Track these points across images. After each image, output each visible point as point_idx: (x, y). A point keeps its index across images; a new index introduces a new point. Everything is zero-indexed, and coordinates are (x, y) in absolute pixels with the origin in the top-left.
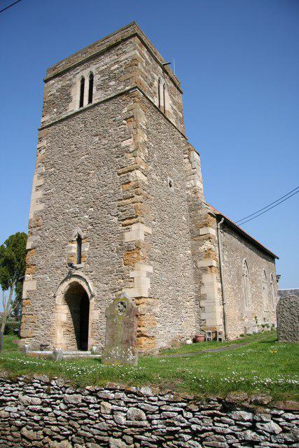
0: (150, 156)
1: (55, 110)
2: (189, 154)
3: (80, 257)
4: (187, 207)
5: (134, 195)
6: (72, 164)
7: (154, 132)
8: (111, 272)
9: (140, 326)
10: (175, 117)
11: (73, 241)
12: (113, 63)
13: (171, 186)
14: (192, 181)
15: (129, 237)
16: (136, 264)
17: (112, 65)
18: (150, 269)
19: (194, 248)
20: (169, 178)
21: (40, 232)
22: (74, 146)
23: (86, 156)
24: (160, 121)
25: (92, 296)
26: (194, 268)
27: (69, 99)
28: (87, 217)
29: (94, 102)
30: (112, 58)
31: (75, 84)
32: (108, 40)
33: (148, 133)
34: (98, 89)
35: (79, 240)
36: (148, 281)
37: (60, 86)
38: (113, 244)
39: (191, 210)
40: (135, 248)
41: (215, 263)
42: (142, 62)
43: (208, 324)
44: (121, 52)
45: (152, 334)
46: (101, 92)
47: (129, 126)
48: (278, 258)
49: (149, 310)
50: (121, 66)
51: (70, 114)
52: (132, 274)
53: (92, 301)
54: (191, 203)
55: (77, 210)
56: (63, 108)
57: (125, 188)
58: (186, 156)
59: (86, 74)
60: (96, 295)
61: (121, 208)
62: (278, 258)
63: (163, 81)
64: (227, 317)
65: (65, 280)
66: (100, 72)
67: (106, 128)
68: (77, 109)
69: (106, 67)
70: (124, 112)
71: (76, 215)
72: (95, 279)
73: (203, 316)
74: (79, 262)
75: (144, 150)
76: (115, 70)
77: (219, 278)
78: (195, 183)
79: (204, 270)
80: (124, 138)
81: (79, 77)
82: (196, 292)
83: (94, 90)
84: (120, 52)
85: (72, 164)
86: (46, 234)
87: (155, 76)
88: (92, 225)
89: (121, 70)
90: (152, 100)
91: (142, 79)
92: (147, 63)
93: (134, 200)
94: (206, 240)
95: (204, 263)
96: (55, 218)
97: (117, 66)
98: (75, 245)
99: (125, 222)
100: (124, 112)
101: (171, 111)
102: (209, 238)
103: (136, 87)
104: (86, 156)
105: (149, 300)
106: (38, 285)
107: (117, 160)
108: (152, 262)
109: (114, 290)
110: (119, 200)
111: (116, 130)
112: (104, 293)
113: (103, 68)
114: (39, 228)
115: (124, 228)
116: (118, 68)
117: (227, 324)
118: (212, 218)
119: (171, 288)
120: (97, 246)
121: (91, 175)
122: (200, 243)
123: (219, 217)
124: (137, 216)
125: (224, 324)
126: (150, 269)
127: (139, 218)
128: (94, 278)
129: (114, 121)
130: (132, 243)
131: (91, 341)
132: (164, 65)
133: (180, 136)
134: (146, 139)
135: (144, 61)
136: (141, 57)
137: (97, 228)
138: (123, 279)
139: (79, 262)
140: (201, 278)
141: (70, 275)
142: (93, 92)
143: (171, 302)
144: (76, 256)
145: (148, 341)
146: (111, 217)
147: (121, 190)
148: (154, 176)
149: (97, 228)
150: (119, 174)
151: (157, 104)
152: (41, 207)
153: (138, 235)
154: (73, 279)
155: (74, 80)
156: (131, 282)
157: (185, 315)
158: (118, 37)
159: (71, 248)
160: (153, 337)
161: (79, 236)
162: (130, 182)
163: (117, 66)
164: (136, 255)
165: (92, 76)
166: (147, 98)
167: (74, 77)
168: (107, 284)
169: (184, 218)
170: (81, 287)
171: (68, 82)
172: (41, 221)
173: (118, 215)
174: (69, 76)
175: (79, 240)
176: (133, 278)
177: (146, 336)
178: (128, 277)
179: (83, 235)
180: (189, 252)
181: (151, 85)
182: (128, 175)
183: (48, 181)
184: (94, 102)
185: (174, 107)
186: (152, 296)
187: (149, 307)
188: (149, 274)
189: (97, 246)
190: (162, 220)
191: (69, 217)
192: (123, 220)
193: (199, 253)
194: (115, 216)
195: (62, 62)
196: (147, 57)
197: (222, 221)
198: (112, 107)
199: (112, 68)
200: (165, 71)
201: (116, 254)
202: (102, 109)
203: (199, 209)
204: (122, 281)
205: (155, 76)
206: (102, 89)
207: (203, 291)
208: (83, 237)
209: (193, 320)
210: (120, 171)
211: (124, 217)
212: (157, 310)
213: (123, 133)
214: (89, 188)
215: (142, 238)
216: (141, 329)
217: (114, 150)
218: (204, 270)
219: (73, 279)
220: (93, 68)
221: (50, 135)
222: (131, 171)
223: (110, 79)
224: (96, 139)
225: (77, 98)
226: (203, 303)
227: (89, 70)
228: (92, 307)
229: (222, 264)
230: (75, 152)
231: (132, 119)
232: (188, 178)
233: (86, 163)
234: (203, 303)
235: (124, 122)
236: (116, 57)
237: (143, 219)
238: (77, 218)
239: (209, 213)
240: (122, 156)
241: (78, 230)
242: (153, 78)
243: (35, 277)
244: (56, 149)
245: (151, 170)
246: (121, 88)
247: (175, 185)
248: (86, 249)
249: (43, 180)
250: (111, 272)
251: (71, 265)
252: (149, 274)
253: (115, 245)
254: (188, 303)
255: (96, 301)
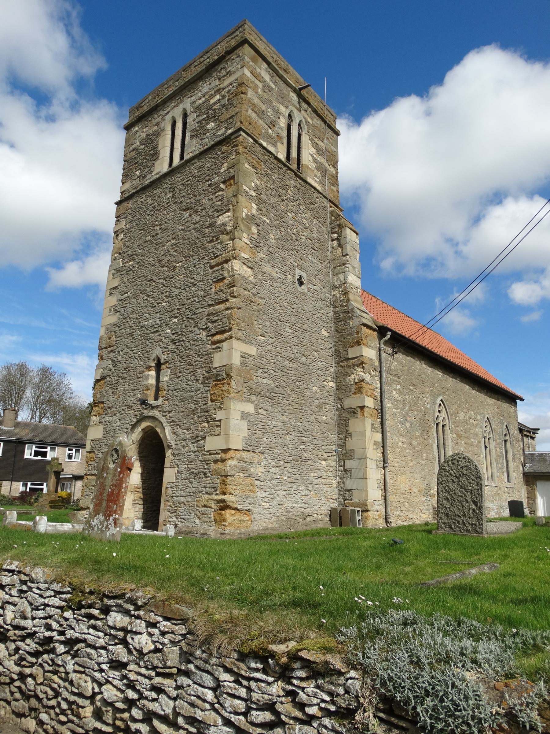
0: (263, 235)
1: (138, 173)
2: (339, 233)
3: (158, 389)
4: (331, 315)
5: (229, 297)
6: (156, 253)
7: (273, 200)
8: (194, 412)
9: (225, 494)
10: (319, 174)
11: (151, 367)
12: (213, 92)
13: (301, 283)
14: (341, 276)
15: (218, 360)
16: (225, 400)
17: (212, 97)
18: (250, 408)
19: (340, 378)
20: (298, 272)
21: (111, 355)
22: (158, 228)
23: (173, 242)
24: (287, 182)
25: (170, 447)
26: (338, 409)
27: (155, 155)
28: (169, 331)
29: (187, 157)
30: (213, 85)
31: (163, 130)
32: (208, 55)
33: (260, 201)
34: (192, 137)
35: (159, 365)
36: (244, 425)
37: (144, 135)
38: (199, 370)
39: (338, 320)
40: (225, 376)
41: (369, 402)
42: (256, 88)
43: (356, 497)
44: (225, 73)
45: (246, 506)
46: (195, 140)
47: (227, 193)
48: (522, 400)
49: (243, 470)
50: (224, 97)
51: (155, 177)
52: (219, 415)
53: (168, 453)
54: (339, 309)
55: (158, 322)
56: (147, 170)
57: (218, 288)
58: (335, 236)
59: (177, 113)
60: (174, 446)
61: (211, 317)
62: (522, 400)
63: (298, 117)
64: (390, 489)
65: (134, 426)
66: (197, 109)
67: (199, 198)
68: (165, 168)
69: (203, 99)
70: (222, 170)
71: (156, 329)
72: (173, 423)
73: (349, 484)
74: (156, 398)
75: (249, 228)
76: (215, 103)
77: (378, 425)
78: (345, 277)
79: (353, 412)
80: (220, 211)
81: (168, 118)
82: (339, 446)
83: (187, 138)
84: (224, 73)
85: (156, 253)
86: (120, 358)
87: (282, 109)
88: (175, 343)
89: (222, 102)
90: (271, 149)
91: (254, 115)
92: (267, 88)
93: (228, 305)
94: (358, 366)
95: (352, 402)
96: (131, 334)
97: (218, 97)
98: (153, 373)
99: (218, 337)
100: (222, 170)
101: (313, 166)
102: (362, 363)
103: (240, 129)
104: (173, 242)
105: (244, 454)
106: (106, 432)
107: (211, 245)
108: (254, 398)
109: (196, 439)
110: (210, 305)
111: (211, 199)
112: (184, 443)
113: (200, 101)
114: (110, 349)
115: (214, 346)
116: (219, 100)
117: (390, 498)
118: (370, 332)
119: (288, 438)
120: (179, 375)
121: (177, 271)
122: (349, 370)
123: (382, 331)
124: (230, 329)
125: (385, 499)
126: (250, 408)
127: (232, 332)
128: (173, 421)
129: (209, 185)
130: (222, 369)
131: (164, 514)
132: (300, 89)
133: (328, 204)
134: (254, 212)
135: (260, 85)
136: (253, 79)
137: (180, 348)
138: (208, 422)
139: (156, 398)
140: (347, 425)
141: (143, 418)
142: (186, 143)
143: (288, 459)
144: (154, 389)
145: (238, 516)
146: (198, 331)
147: (213, 290)
148: (267, 268)
149: (180, 348)
150: (212, 267)
151: (282, 156)
152: (114, 319)
153: (230, 356)
154: (144, 425)
155: (162, 125)
156: (217, 426)
157: (315, 481)
158: (222, 47)
159: (147, 377)
160: (248, 510)
161: (159, 360)
162: (224, 278)
163: (218, 97)
164: (225, 387)
165: (185, 116)
166: (261, 145)
167: (163, 119)
168: (188, 430)
169: (324, 332)
170: (157, 433)
171: (156, 128)
172: (113, 338)
173: (207, 328)
174: (156, 118)
175: (159, 365)
176: (220, 421)
177: (236, 509)
178: (215, 420)
179: (163, 358)
180: (332, 384)
181: (272, 124)
182: (222, 268)
183: (125, 280)
184: (187, 157)
185: (320, 159)
186: (249, 448)
187: (242, 464)
188: (244, 416)
189: (179, 375)
190: (278, 335)
191: (148, 332)
192: (213, 335)
193: (347, 385)
194: (203, 329)
195: (149, 95)
196: (267, 78)
197: (388, 337)
198: (208, 165)
199: (212, 101)
200: (300, 96)
201: (202, 386)
202: (195, 169)
203: (351, 318)
204: (206, 425)
205: (282, 109)
206: (197, 136)
207: (351, 444)
208: (162, 361)
209: (332, 490)
210: (213, 262)
211: (214, 331)
212: (260, 470)
213: (219, 203)
214: (174, 289)
215: (236, 360)
216: (227, 497)
217: (207, 230)
218: (353, 412)
219: (144, 425)
220: (187, 104)
221: (130, 211)
222: (226, 261)
223: (208, 120)
224: (186, 215)
225: (165, 153)
226: (349, 464)
227: (181, 106)
228: (168, 462)
229: (388, 404)
230: (159, 236)
231: (232, 181)
232: (336, 271)
233: (172, 252)
234: (349, 464)
235: (222, 186)
236: (217, 82)
237: (240, 334)
238: (157, 334)
239: (365, 325)
240: (217, 239)
241: (157, 351)
242: (277, 113)
243: (103, 420)
244: (136, 234)
245: (262, 259)
246: (221, 132)
247: (310, 282)
248: (166, 379)
249: (119, 278)
250: (194, 412)
251: (143, 402)
252: (244, 416)
253: (201, 373)
254: (323, 463)
255: (173, 454)
